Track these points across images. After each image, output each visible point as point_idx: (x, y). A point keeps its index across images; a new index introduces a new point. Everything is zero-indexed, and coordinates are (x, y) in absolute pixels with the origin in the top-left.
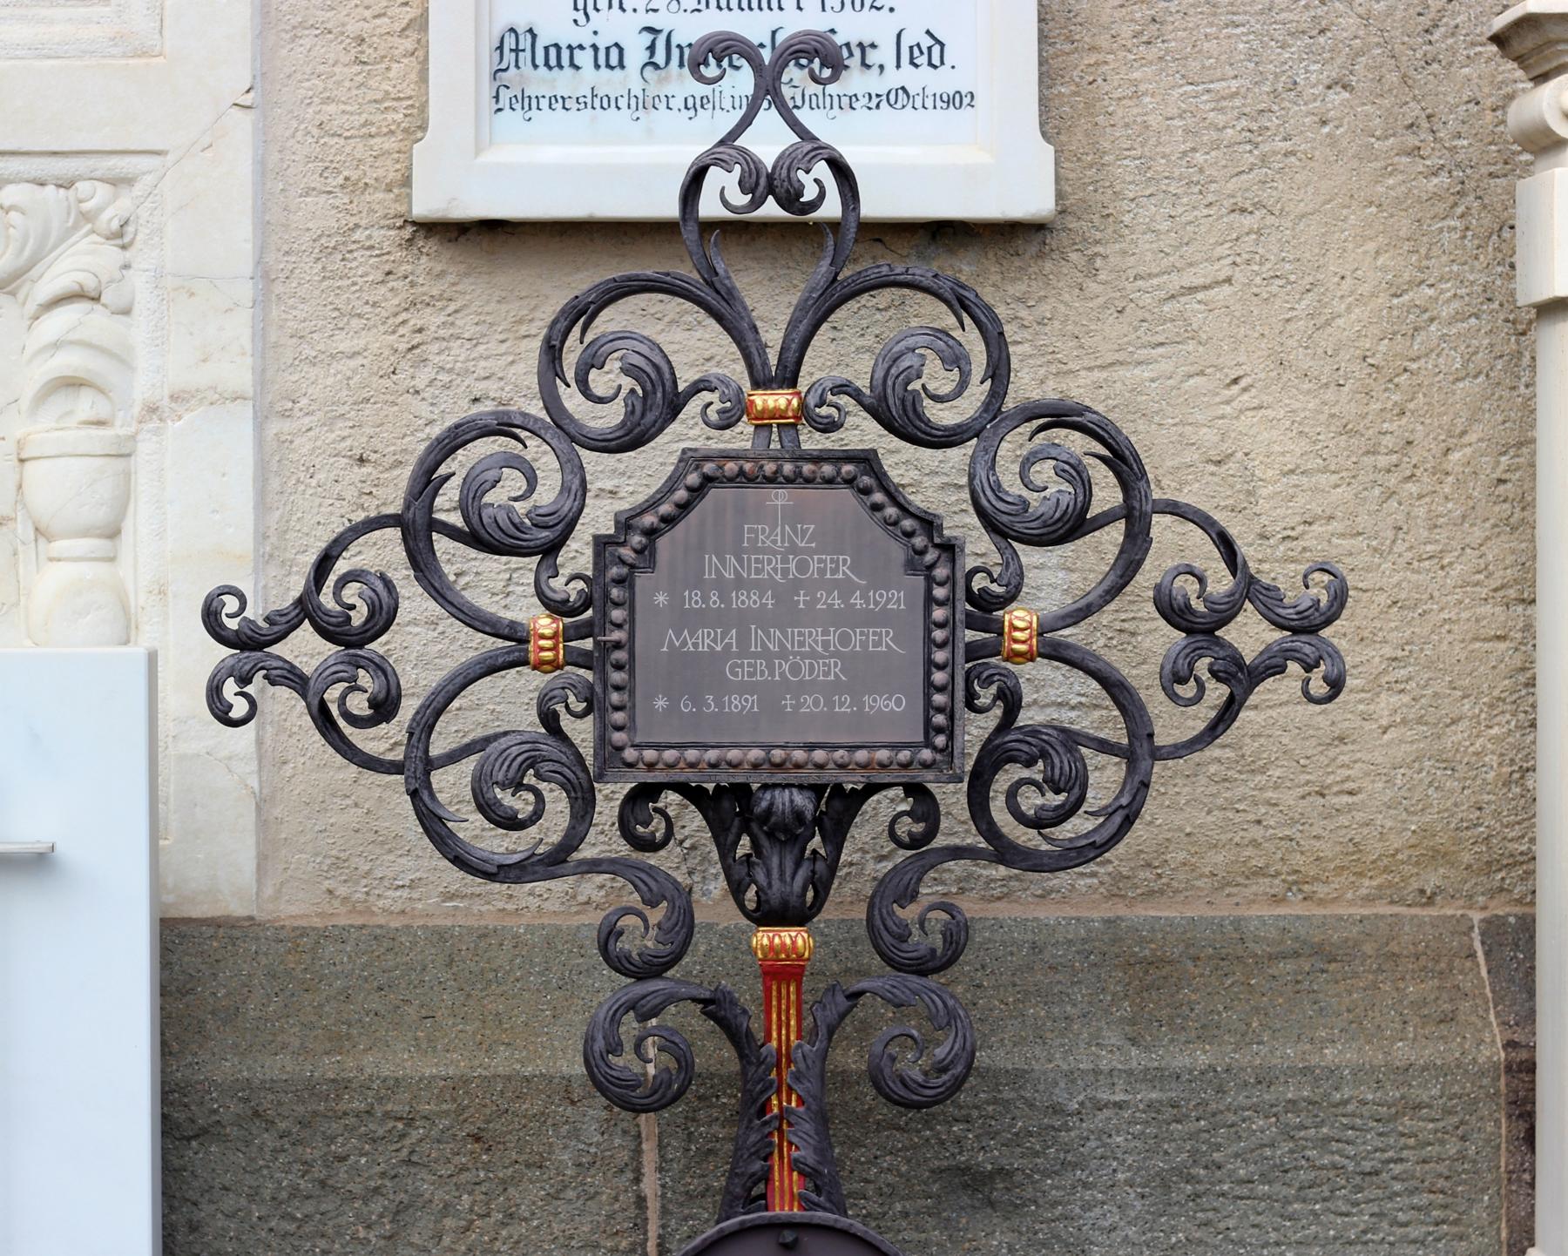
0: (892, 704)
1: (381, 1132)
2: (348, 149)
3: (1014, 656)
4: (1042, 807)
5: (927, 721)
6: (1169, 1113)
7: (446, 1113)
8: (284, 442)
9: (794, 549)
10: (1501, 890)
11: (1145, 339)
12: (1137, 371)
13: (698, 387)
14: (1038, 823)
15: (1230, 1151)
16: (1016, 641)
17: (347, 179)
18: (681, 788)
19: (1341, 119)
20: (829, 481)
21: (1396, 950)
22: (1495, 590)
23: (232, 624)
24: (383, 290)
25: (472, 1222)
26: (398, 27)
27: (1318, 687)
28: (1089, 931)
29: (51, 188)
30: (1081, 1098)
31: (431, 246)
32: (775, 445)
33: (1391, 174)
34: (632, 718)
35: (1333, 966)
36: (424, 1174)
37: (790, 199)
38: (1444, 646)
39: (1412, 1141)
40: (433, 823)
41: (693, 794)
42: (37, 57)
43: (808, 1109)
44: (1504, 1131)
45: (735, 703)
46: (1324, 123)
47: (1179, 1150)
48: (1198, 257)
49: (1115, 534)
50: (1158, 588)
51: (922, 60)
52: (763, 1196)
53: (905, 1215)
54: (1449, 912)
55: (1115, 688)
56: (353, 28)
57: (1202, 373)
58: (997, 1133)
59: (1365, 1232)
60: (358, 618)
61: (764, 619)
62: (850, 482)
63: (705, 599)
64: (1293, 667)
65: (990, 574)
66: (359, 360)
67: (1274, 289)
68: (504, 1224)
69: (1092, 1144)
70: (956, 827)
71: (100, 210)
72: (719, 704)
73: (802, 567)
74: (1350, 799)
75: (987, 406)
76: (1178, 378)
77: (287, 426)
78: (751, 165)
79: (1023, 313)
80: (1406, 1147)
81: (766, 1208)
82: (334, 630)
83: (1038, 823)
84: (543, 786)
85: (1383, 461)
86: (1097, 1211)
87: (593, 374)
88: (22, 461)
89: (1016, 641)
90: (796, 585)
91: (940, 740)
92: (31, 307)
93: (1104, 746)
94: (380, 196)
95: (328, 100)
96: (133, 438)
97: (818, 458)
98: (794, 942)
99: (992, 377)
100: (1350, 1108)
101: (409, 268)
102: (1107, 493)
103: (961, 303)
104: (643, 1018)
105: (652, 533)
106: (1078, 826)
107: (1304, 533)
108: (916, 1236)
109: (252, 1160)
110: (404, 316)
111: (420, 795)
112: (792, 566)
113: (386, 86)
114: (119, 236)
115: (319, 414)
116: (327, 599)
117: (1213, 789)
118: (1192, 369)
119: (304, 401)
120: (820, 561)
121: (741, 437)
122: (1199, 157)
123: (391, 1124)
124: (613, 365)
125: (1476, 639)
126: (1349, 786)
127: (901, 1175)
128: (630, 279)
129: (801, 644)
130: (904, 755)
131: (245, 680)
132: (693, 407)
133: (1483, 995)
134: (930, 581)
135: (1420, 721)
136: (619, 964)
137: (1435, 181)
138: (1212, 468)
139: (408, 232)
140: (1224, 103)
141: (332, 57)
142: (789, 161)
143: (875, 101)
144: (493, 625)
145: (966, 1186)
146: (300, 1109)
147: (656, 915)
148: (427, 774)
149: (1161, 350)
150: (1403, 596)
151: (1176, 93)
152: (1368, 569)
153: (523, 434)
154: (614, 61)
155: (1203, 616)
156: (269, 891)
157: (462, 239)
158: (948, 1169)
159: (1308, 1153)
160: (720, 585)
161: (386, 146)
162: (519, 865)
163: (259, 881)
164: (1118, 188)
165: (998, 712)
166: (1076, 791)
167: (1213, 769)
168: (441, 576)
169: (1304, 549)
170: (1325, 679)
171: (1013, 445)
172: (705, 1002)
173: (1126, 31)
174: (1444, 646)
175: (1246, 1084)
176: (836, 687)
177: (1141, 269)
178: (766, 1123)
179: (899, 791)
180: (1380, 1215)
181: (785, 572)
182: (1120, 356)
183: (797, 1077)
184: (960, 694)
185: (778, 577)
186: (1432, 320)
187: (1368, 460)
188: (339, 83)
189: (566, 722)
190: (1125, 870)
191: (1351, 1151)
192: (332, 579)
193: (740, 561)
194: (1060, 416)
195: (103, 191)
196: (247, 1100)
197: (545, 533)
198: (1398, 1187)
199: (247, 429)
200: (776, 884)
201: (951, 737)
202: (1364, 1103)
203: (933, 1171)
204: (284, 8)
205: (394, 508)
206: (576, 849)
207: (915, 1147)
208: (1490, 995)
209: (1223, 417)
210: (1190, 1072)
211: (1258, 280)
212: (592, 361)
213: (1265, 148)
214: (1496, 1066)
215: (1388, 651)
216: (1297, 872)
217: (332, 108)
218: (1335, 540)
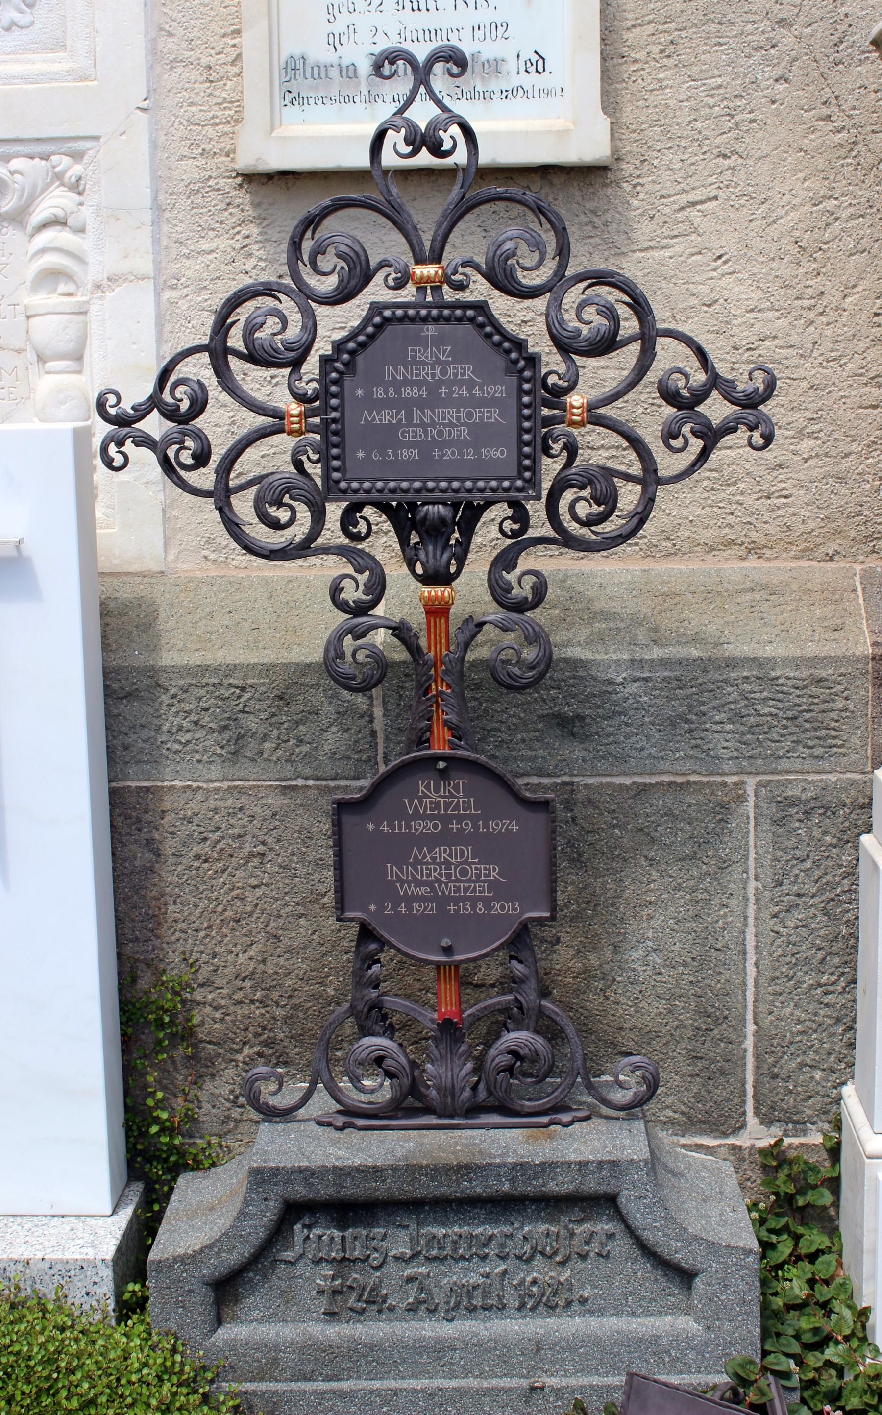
0: (498, 454)
1: (227, 695)
2: (204, 132)
3: (572, 424)
4: (590, 514)
5: (520, 463)
6: (675, 683)
7: (263, 684)
8: (173, 303)
9: (438, 362)
10: (873, 552)
11: (667, 233)
12: (662, 253)
13: (381, 266)
14: (588, 523)
15: (710, 705)
16: (574, 415)
17: (204, 150)
18: (377, 504)
19: (783, 99)
20: (459, 320)
21: (811, 587)
22: (872, 378)
23: (113, 411)
24: (226, 214)
25: (279, 744)
26: (230, 59)
27: (758, 440)
28: (633, 576)
29: (37, 160)
30: (624, 675)
31: (254, 187)
32: (429, 299)
33: (813, 132)
34: (344, 463)
35: (773, 598)
36: (251, 717)
37: (437, 150)
38: (841, 412)
39: (816, 701)
40: (233, 526)
41: (383, 507)
42: (26, 83)
43: (453, 691)
44: (870, 694)
45: (405, 454)
46: (773, 102)
47: (681, 705)
48: (697, 184)
49: (635, 347)
50: (660, 382)
51: (532, 69)
52: (428, 741)
53: (523, 741)
54: (843, 565)
55: (636, 443)
56: (205, 61)
57: (700, 253)
58: (576, 695)
59: (788, 751)
60: (185, 406)
61: (421, 404)
62: (472, 320)
63: (386, 392)
64: (743, 428)
65: (558, 375)
66: (215, 255)
67: (742, 202)
68: (298, 746)
69: (631, 701)
70: (539, 526)
71: (64, 172)
72: (396, 455)
73: (444, 372)
74: (785, 501)
75: (555, 274)
76: (686, 256)
77: (175, 294)
78: (412, 128)
79: (595, 219)
80: (813, 703)
81: (429, 748)
82: (171, 414)
83: (588, 523)
84: (294, 504)
85: (806, 303)
86: (634, 739)
87: (319, 257)
88: (28, 317)
89: (574, 415)
90: (440, 383)
91: (527, 474)
92: (30, 229)
93: (628, 477)
94: (223, 159)
95: (192, 104)
96: (88, 302)
97: (453, 306)
98: (443, 594)
99: (559, 255)
100: (781, 681)
101: (240, 201)
102: (630, 325)
103: (539, 210)
104: (356, 638)
105: (353, 353)
106: (609, 527)
107: (759, 346)
108: (529, 753)
109: (157, 710)
110: (239, 228)
111: (224, 509)
112: (438, 372)
113: (224, 95)
114: (77, 187)
115: (192, 287)
116: (167, 397)
117: (706, 495)
118: (694, 250)
119: (183, 280)
120: (454, 368)
121: (408, 294)
122: (698, 125)
123: (233, 690)
124: (331, 250)
125: (861, 407)
126: (784, 493)
127: (521, 719)
128: (339, 199)
129: (444, 418)
130: (506, 484)
131: (120, 443)
132: (379, 278)
133: (860, 614)
134: (522, 380)
135: (826, 455)
136: (342, 606)
137: (840, 136)
138: (706, 308)
139: (239, 180)
140: (713, 92)
141: (193, 78)
142: (434, 126)
143: (505, 94)
144: (264, 409)
145: (558, 724)
146: (182, 682)
147: (363, 578)
148: (229, 497)
149: (675, 240)
150: (817, 382)
151: (685, 86)
152: (796, 367)
153: (280, 295)
154: (351, 74)
155: (687, 398)
156: (171, 557)
157: (270, 183)
158: (547, 715)
159: (756, 707)
160: (394, 383)
161: (226, 129)
162: (282, 550)
163: (165, 551)
164: (650, 144)
165: (565, 454)
166: (610, 504)
167: (705, 483)
168: (233, 380)
169: (760, 356)
170: (762, 436)
171: (573, 296)
172: (394, 629)
173: (655, 49)
174: (841, 412)
175: (720, 667)
176: (466, 444)
177: (664, 192)
178: (428, 699)
179: (505, 505)
180: (797, 742)
181: (433, 375)
182: (652, 244)
183: (446, 672)
184: (539, 447)
185: (429, 379)
186: (836, 219)
187: (798, 303)
188: (197, 94)
189: (307, 465)
190: (654, 542)
191: (780, 705)
192: (169, 384)
193: (406, 369)
194: (600, 278)
195: (66, 160)
196: (151, 677)
197: (293, 354)
198: (807, 726)
199: (151, 296)
200: (431, 561)
201: (534, 473)
202: (788, 678)
203: (539, 716)
204: (165, 50)
205: (206, 341)
206: (315, 540)
207: (529, 703)
208: (864, 615)
209: (712, 278)
210: (688, 660)
211: (733, 197)
212: (319, 251)
213: (737, 118)
214: (867, 657)
215: (808, 415)
216: (754, 542)
217: (193, 109)
218: (777, 350)
